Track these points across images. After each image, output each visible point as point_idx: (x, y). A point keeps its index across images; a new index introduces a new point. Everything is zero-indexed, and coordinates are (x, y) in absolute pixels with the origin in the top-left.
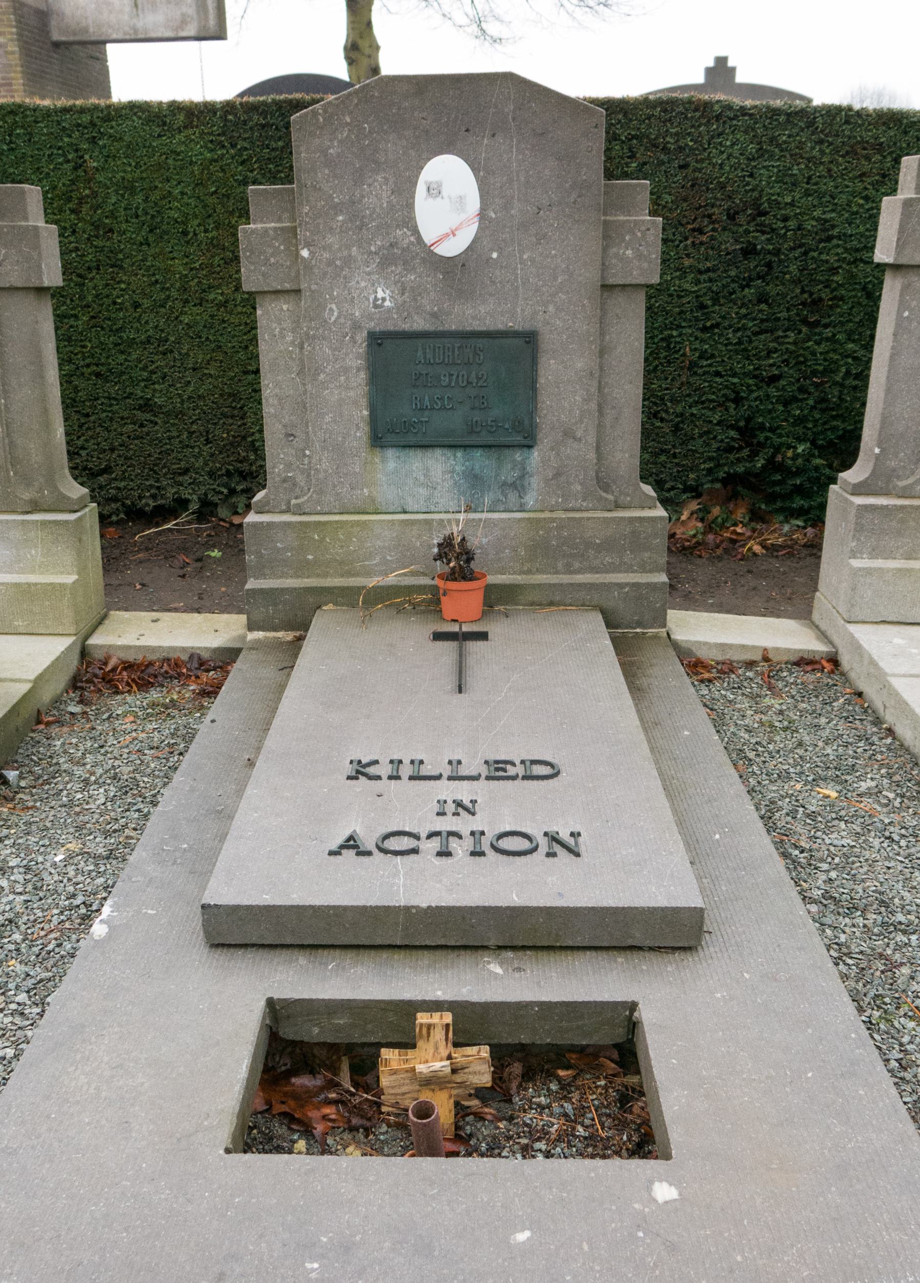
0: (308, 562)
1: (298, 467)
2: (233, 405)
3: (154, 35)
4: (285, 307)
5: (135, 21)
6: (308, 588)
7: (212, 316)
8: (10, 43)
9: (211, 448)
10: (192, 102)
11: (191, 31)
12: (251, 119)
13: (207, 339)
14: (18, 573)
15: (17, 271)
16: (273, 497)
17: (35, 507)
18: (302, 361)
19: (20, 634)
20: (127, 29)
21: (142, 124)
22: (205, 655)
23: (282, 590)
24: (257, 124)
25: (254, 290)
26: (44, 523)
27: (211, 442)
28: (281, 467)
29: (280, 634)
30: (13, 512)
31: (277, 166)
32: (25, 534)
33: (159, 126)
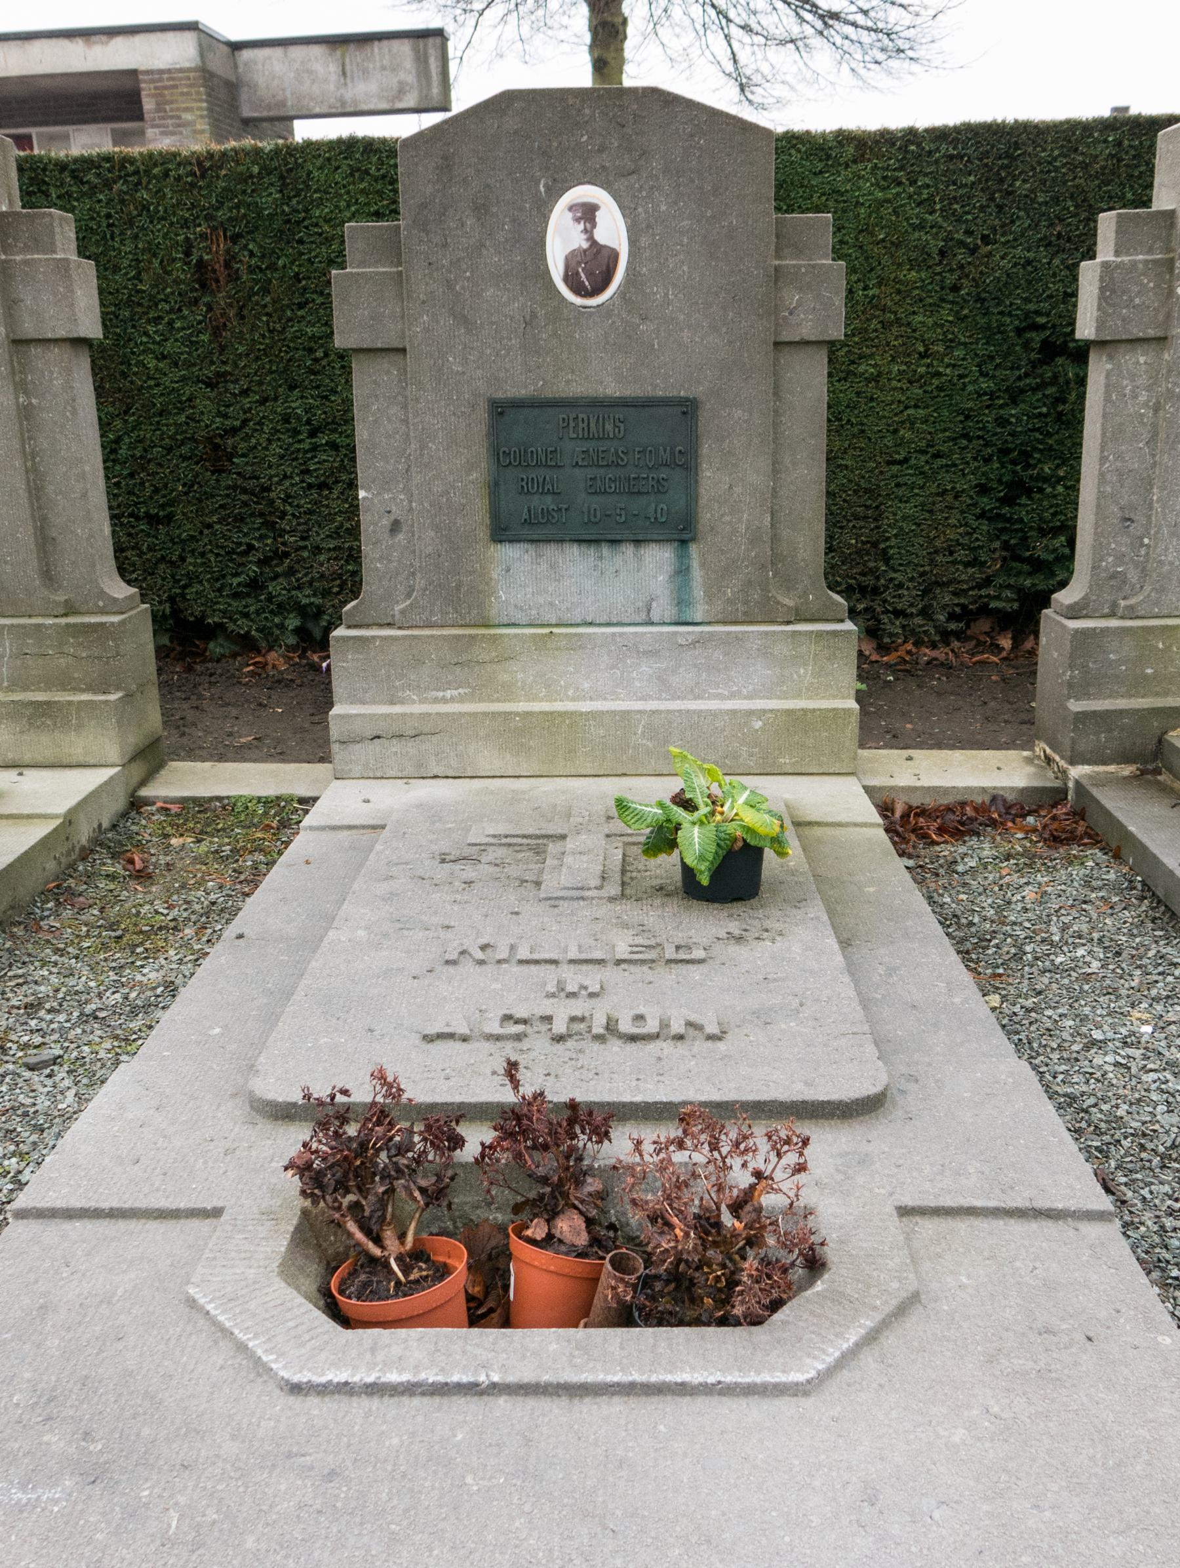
0: (1146, 677)
1: (1132, 559)
2: (869, 502)
3: (365, 107)
4: (1142, 360)
5: (342, 91)
6: (1153, 709)
7: (858, 394)
8: (199, 120)
9: (833, 557)
10: (946, 126)
11: (410, 101)
12: (938, 150)
13: (849, 421)
14: (779, 698)
15: (811, 320)
16: (1094, 598)
17: (800, 617)
18: (1154, 426)
19: (785, 774)
20: (332, 100)
21: (802, 158)
22: (1010, 797)
23: (1121, 711)
24: (944, 156)
25: (1109, 338)
26: (820, 634)
27: (834, 551)
28: (1110, 559)
29: (1112, 768)
30: (773, 622)
31: (963, 206)
32: (794, 649)
33: (821, 160)
